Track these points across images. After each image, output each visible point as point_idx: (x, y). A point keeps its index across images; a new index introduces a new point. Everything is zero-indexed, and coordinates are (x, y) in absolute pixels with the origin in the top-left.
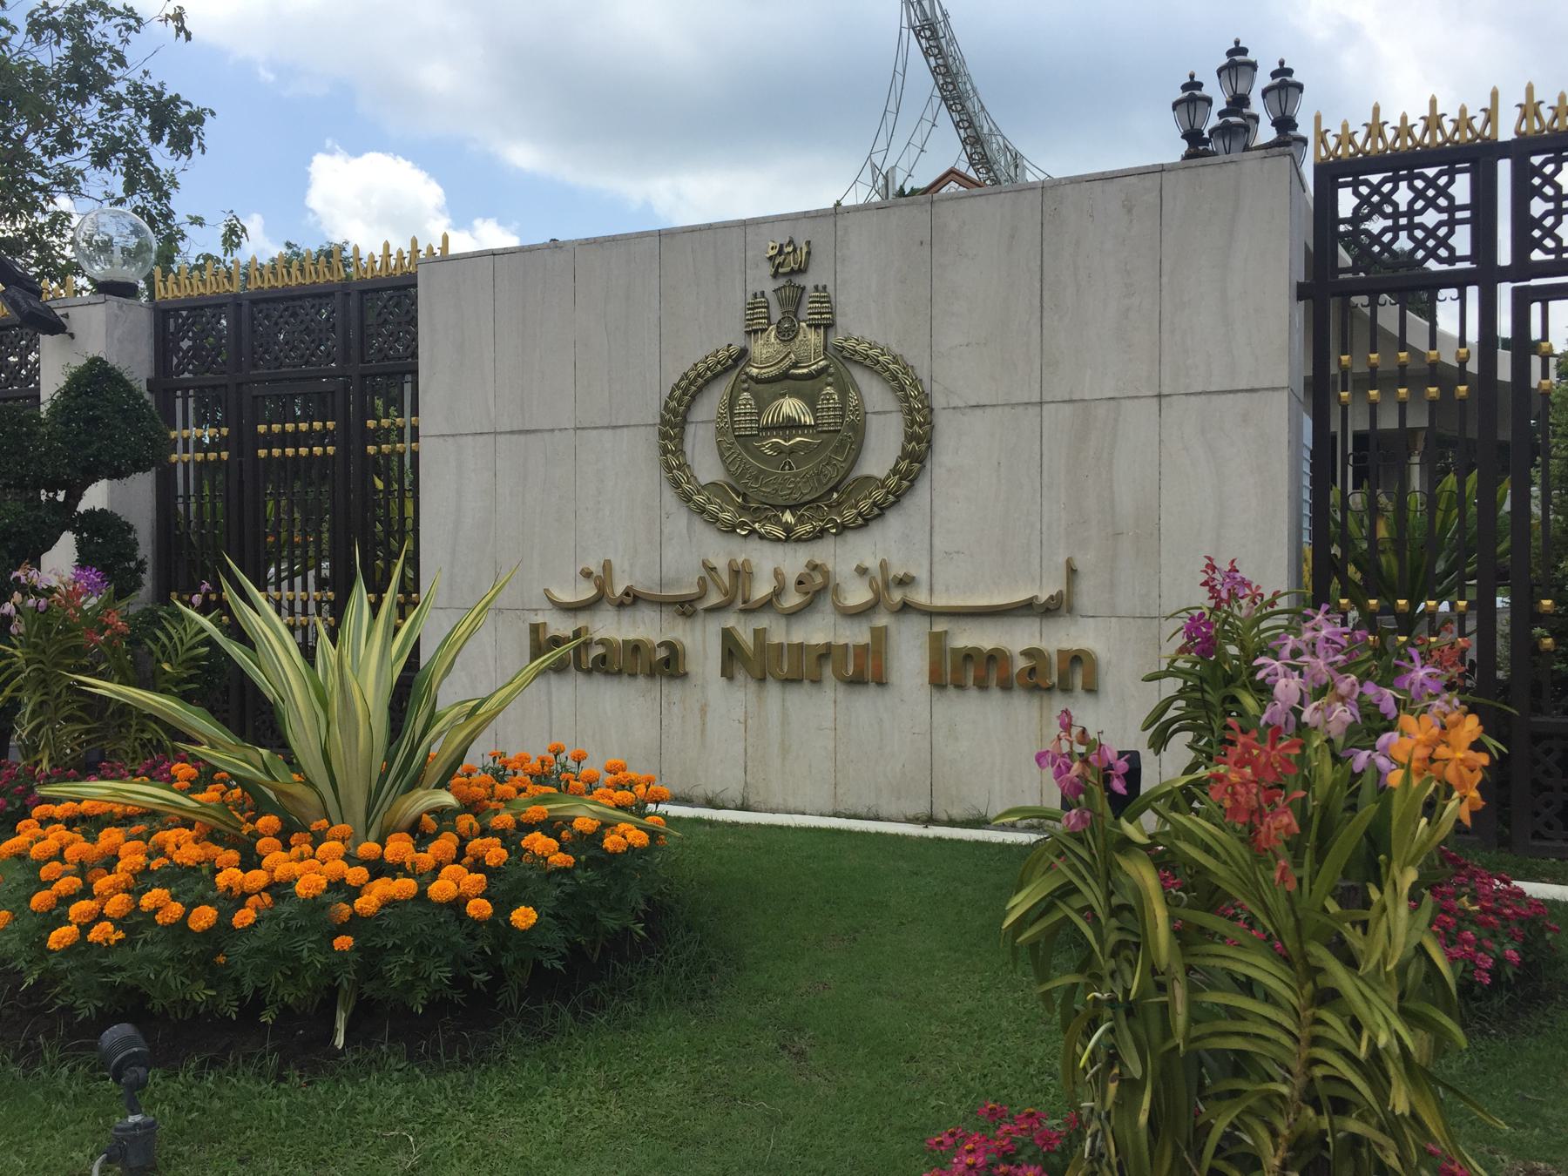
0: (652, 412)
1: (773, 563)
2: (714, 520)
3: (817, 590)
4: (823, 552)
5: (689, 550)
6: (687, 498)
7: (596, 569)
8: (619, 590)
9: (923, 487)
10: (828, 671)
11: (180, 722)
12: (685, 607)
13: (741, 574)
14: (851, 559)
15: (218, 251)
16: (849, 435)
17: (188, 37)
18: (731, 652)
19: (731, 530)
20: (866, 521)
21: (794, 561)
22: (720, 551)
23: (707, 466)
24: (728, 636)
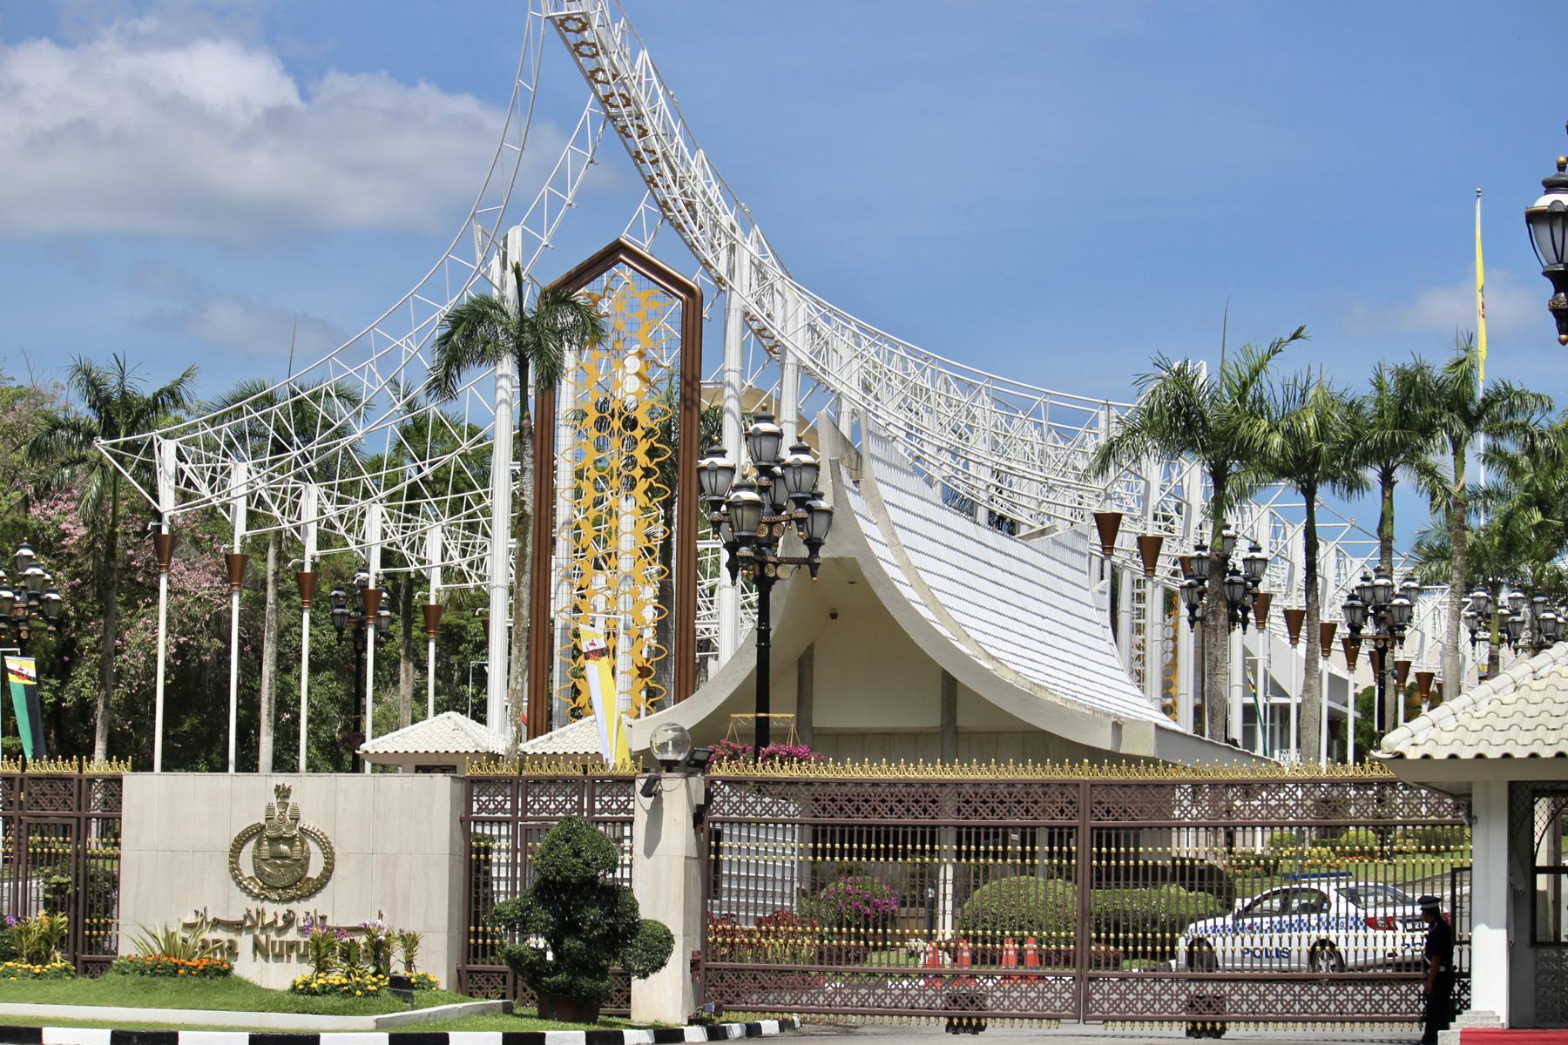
0: (228, 847)
1: (274, 911)
2: (250, 893)
3: (289, 920)
4: (294, 906)
5: (238, 906)
6: (239, 883)
7: (201, 911)
8: (210, 919)
9: (330, 884)
10: (294, 955)
11: (128, 1023)
12: (237, 927)
13: (261, 914)
14: (300, 909)
15: (318, 796)
16: (304, 863)
17: (1301, 329)
18: (257, 946)
19: (257, 897)
20: (311, 894)
21: (282, 909)
22: (254, 905)
23: (247, 869)
24: (256, 939)
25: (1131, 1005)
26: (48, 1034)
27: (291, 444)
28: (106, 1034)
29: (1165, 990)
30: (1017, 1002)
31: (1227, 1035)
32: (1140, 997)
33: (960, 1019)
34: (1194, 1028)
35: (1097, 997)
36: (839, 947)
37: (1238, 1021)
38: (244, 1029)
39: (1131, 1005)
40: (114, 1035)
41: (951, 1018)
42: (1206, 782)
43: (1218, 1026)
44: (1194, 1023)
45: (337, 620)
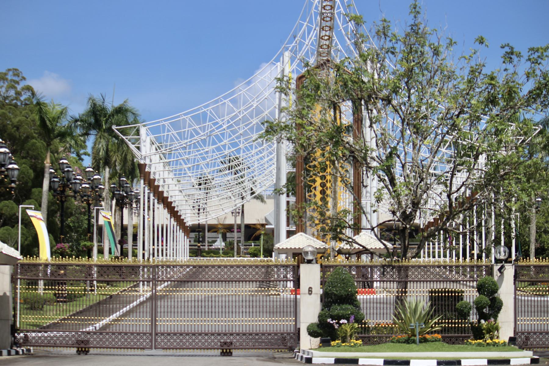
11: (450, 358)
25: (184, 344)
26: (463, 362)
27: (189, 119)
28: (435, 362)
29: (104, 337)
30: (129, 343)
31: (90, 352)
32: (175, 341)
33: (226, 350)
34: (223, 351)
35: (148, 341)
36: (461, 327)
37: (94, 348)
38: (485, 358)
39: (184, 344)
40: (439, 363)
41: (223, 350)
42: (532, 265)
43: (87, 349)
44: (223, 350)
45: (112, 189)
